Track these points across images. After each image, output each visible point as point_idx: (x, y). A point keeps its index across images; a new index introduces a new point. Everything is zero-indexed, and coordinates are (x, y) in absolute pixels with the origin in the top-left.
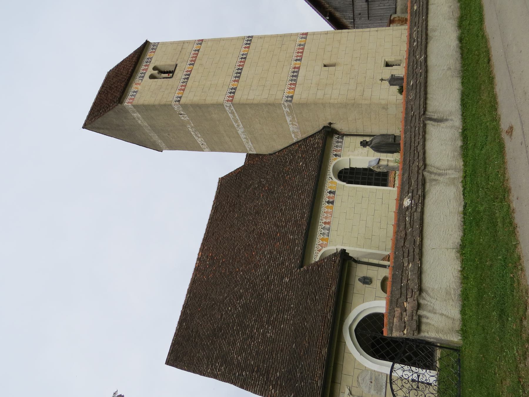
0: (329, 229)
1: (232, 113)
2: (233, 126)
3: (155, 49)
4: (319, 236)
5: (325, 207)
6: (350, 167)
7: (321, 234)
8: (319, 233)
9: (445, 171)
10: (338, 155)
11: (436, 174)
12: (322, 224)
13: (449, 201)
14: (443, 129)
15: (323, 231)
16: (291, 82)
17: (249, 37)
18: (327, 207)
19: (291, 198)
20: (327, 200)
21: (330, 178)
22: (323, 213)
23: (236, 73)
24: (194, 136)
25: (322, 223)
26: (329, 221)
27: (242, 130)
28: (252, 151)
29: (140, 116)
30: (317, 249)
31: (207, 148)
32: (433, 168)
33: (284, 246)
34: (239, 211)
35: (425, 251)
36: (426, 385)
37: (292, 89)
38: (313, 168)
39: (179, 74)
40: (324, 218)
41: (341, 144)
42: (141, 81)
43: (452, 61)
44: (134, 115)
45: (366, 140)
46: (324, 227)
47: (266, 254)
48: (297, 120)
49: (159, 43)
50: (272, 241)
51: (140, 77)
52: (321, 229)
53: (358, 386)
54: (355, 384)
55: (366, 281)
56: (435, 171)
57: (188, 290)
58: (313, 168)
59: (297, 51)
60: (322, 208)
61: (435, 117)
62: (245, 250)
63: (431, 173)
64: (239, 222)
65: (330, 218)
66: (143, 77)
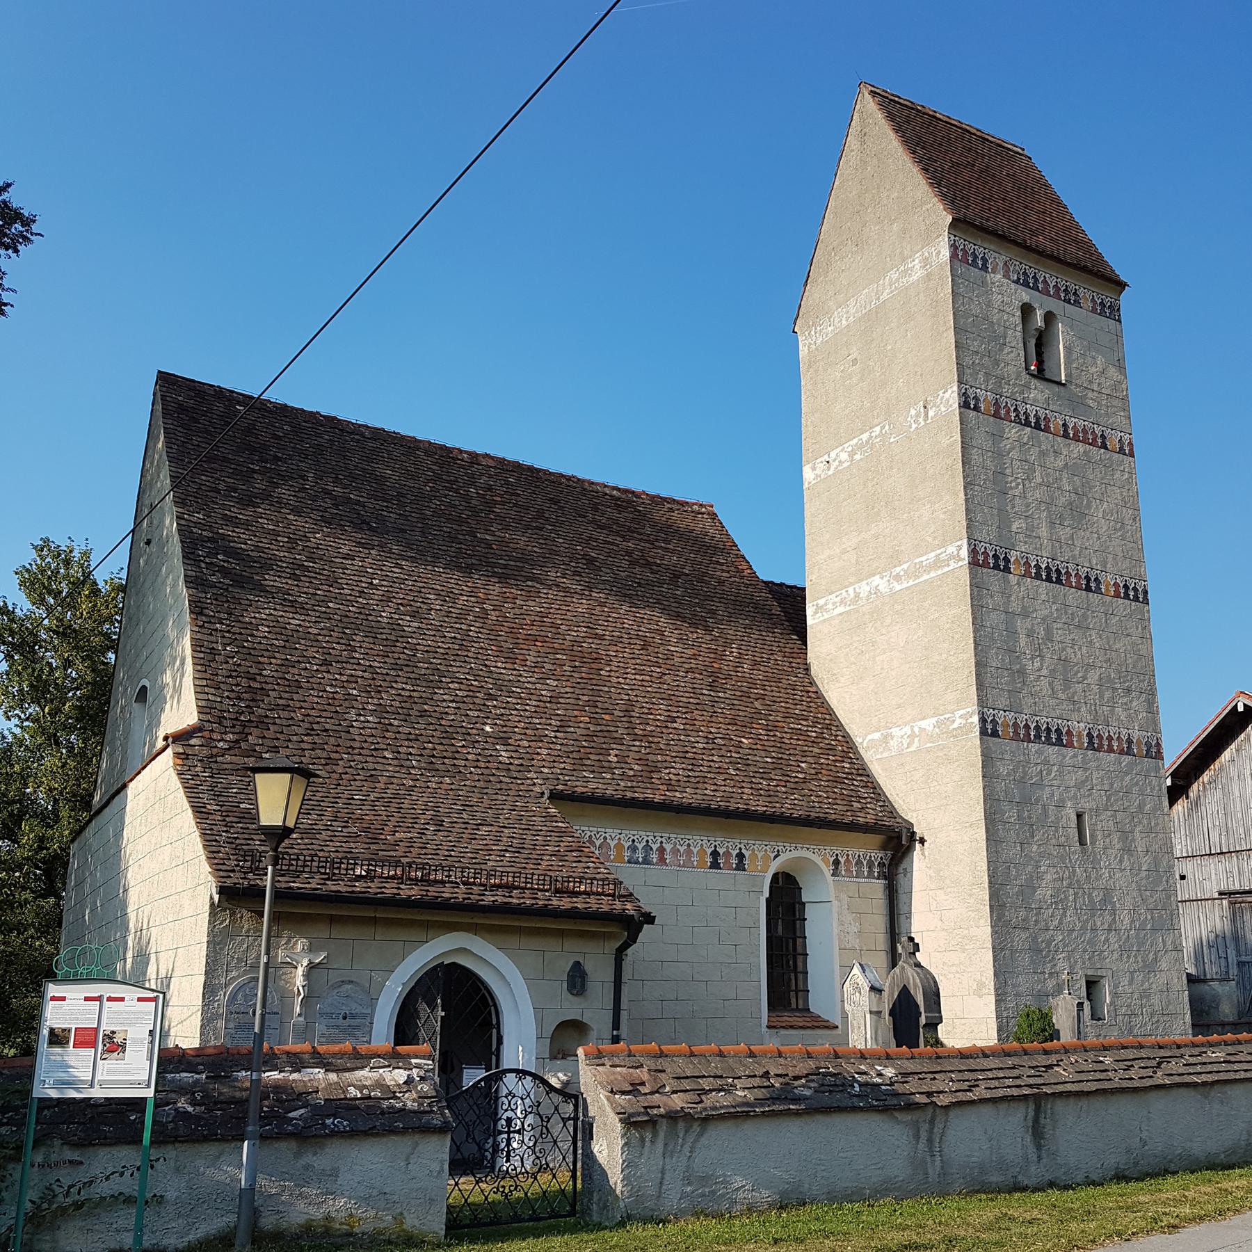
0: (646, 861)
1: (938, 563)
2: (895, 559)
3: (1102, 313)
4: (626, 835)
5: (702, 845)
6: (804, 904)
7: (633, 841)
8: (634, 835)
9: (939, 1152)
10: (837, 868)
11: (931, 1131)
12: (659, 841)
13: (879, 1166)
14: (1020, 1140)
15: (640, 846)
16: (1032, 728)
17: (1145, 592)
18: (702, 851)
19: (710, 746)
20: (721, 851)
21: (778, 851)
22: (687, 842)
23: (1047, 567)
24: (855, 441)
25: (662, 842)
26: (668, 861)
27: (883, 588)
28: (816, 613)
29: (915, 278)
30: (592, 834)
31: (817, 476)
32: (941, 1126)
33: (585, 738)
34: (636, 583)
35: (778, 1123)
36: (506, 1149)
37: (1016, 733)
38: (800, 803)
39: (1037, 396)
40: (675, 844)
41: (866, 873)
42: (1015, 278)
43: (1160, 1148)
44: (917, 261)
45: (919, 951)
46: (651, 849)
47: (547, 684)
48: (928, 751)
49: (1120, 322)
50: (586, 698)
51: (1025, 273)
52: (644, 840)
53: (332, 986)
54: (334, 977)
55: (577, 980)
56: (935, 1130)
57: (379, 429)
58: (800, 803)
59: (1114, 734)
60: (699, 837)
61: (1042, 1121)
62: (540, 614)
63: (932, 1122)
64: (608, 587)
65: (676, 862)
66: (1026, 284)
